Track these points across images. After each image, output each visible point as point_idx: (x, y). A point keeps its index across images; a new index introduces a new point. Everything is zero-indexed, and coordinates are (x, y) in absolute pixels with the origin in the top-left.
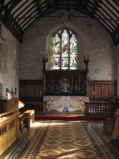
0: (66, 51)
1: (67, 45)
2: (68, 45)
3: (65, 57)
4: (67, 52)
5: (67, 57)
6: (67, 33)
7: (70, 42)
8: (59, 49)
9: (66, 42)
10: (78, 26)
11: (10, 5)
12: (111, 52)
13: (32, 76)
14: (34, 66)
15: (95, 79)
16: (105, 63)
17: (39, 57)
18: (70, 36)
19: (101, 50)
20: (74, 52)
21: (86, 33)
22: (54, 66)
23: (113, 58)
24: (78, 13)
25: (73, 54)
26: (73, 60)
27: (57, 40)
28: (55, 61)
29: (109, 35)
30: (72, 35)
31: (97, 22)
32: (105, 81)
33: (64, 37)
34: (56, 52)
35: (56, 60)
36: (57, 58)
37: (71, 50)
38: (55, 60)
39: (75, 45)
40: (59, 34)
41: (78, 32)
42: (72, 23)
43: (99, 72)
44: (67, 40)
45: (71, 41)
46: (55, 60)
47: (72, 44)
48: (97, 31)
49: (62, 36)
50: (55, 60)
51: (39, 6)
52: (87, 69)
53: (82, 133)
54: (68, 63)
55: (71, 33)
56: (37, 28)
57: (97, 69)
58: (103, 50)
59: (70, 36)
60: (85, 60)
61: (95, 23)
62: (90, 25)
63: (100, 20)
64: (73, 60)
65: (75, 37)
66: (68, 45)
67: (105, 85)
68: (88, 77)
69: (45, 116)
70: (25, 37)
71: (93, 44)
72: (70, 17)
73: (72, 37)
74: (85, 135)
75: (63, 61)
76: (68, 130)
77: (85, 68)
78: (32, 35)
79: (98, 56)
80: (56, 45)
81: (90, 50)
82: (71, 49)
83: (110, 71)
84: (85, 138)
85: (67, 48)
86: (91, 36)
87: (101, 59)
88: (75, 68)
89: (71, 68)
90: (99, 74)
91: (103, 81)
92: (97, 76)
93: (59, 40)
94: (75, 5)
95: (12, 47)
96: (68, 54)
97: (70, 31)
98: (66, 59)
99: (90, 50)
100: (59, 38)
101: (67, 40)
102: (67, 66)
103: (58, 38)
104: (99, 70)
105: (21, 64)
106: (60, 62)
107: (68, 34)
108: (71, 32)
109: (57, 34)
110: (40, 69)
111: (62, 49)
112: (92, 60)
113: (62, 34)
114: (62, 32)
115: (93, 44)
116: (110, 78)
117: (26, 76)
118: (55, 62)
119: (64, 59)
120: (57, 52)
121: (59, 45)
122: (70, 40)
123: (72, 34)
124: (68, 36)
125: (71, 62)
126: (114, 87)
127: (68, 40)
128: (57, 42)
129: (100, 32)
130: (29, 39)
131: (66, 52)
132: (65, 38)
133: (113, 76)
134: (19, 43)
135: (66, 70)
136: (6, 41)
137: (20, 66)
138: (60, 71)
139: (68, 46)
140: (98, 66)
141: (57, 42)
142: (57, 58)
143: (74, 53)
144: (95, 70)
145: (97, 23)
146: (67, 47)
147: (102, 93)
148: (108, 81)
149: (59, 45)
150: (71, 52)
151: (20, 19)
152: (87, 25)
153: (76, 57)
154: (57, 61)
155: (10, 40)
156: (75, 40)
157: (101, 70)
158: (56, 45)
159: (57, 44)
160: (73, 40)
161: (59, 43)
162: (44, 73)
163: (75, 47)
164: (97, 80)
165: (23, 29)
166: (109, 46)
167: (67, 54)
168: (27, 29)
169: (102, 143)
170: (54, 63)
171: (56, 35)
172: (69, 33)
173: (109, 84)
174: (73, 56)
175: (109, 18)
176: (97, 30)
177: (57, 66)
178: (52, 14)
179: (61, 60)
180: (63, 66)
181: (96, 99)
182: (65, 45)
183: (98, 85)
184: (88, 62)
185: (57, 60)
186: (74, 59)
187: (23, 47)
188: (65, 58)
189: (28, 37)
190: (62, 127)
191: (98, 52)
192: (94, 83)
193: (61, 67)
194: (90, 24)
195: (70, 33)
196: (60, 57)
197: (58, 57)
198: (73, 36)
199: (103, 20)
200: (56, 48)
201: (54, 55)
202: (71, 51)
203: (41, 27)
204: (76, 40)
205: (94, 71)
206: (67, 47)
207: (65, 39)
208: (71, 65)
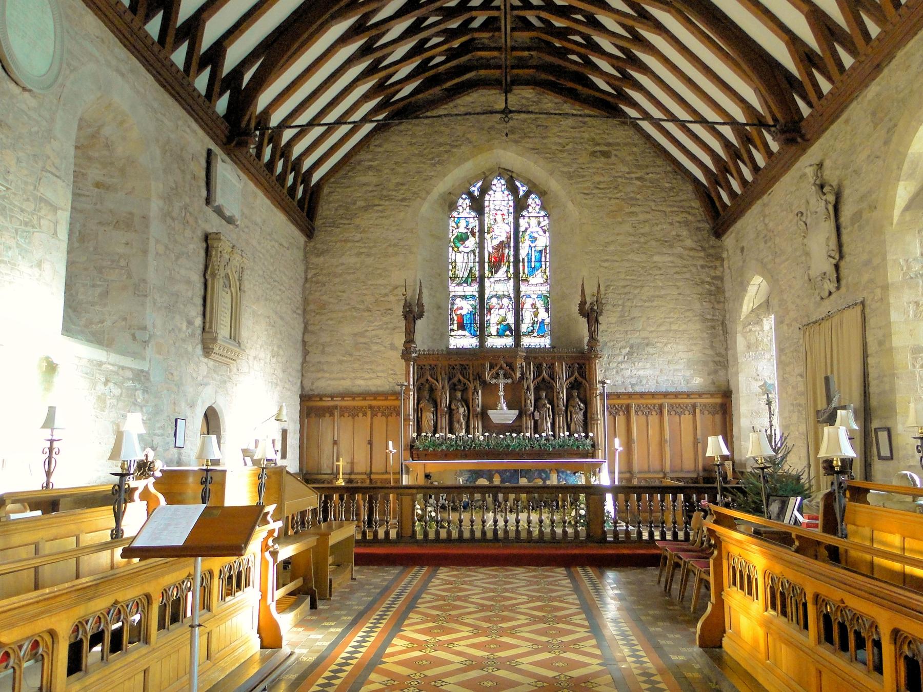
0: (504, 269)
1: (509, 243)
2: (512, 245)
3: (502, 293)
4: (507, 271)
5: (508, 296)
7: (522, 229)
9: (501, 231)
10: (553, 162)
11: (249, 69)
12: (703, 267)
13: (356, 378)
14: (368, 334)
16: (676, 316)
17: (386, 295)
18: (520, 206)
19: (656, 258)
21: (589, 188)
22: (453, 333)
23: (710, 293)
24: (550, 102)
25: (532, 280)
26: (534, 306)
27: (463, 224)
28: (459, 312)
29: (687, 193)
30: (530, 201)
31: (636, 138)
32: (676, 395)
33: (492, 207)
34: (462, 273)
35: (462, 308)
36: (465, 297)
37: (526, 264)
39: (543, 241)
40: (470, 195)
41: (554, 185)
42: (527, 145)
43: (649, 354)
44: (506, 221)
45: (523, 223)
46: (455, 307)
47: (527, 237)
48: (637, 179)
49: (486, 203)
50: (455, 307)
51: (382, 74)
52: (593, 339)
53: (566, 619)
54: (511, 319)
55: (522, 190)
57: (639, 341)
58: (667, 259)
59: (520, 206)
60: (585, 303)
61: (626, 144)
62: (606, 154)
63: (646, 125)
64: (534, 306)
65: (543, 208)
66: (512, 245)
67: (679, 410)
68: (599, 378)
70: (326, 210)
72: (510, 116)
73: (530, 209)
74: (578, 629)
75: (490, 310)
76: (506, 608)
77: (586, 339)
78: (355, 204)
79: (642, 287)
80: (458, 245)
81: (607, 260)
82: (526, 260)
84: (575, 642)
85: (509, 256)
86: (610, 199)
87: (658, 296)
88: (542, 339)
89: (526, 341)
90: (648, 365)
91: (666, 395)
92: (641, 372)
93: (474, 223)
95: (267, 251)
97: (520, 182)
98: (505, 301)
99: (607, 260)
100: (473, 214)
101: (506, 221)
102: (508, 333)
104: (647, 345)
105: (309, 328)
106: (477, 318)
107: (511, 197)
108: (524, 188)
109: (464, 196)
111: (486, 260)
113: (487, 197)
114: (484, 190)
116: (697, 382)
117: (330, 379)
119: (494, 301)
120: (466, 275)
121: (471, 243)
122: (521, 221)
123: (527, 195)
124: (511, 203)
125: (527, 316)
126: (718, 418)
127: (511, 219)
128: (465, 231)
129: (651, 182)
130: (341, 218)
131: (501, 274)
132: (499, 212)
133: (716, 372)
134: (301, 239)
135: (504, 350)
136: (237, 226)
137: (304, 334)
138: (481, 353)
139: (509, 247)
140: (644, 329)
141: (462, 230)
142: (465, 297)
143: (538, 278)
144: (631, 347)
145: (635, 145)
147: (667, 447)
148: (688, 395)
149: (471, 243)
151: (304, 130)
152: (593, 154)
153: (545, 293)
154: (464, 312)
155: (259, 220)
156: (541, 219)
157: (658, 345)
158: (458, 245)
159: (462, 239)
160: (534, 222)
161: (473, 234)
162: (408, 366)
163: (541, 252)
164: (638, 389)
165: (316, 177)
166: (689, 243)
168: (332, 176)
169: (650, 665)
170: (452, 319)
171: (461, 201)
172: (513, 190)
173: (694, 406)
174: (533, 288)
175: (682, 115)
176: (637, 175)
177: (466, 333)
178: (441, 111)
179: (482, 307)
180: (490, 335)
181: (640, 472)
182: (496, 242)
183: (645, 411)
184: (599, 313)
185: (465, 307)
186: (540, 304)
187: (318, 256)
188: (499, 297)
189: (336, 210)
190: (479, 596)
191: (643, 267)
193: (482, 340)
194: (606, 149)
195: (521, 193)
196: (476, 294)
197: (467, 293)
198: (534, 205)
199: (656, 123)
200: (459, 258)
201: (454, 289)
202: (524, 269)
204: (547, 222)
205: (628, 349)
207: (499, 218)
208: (524, 328)
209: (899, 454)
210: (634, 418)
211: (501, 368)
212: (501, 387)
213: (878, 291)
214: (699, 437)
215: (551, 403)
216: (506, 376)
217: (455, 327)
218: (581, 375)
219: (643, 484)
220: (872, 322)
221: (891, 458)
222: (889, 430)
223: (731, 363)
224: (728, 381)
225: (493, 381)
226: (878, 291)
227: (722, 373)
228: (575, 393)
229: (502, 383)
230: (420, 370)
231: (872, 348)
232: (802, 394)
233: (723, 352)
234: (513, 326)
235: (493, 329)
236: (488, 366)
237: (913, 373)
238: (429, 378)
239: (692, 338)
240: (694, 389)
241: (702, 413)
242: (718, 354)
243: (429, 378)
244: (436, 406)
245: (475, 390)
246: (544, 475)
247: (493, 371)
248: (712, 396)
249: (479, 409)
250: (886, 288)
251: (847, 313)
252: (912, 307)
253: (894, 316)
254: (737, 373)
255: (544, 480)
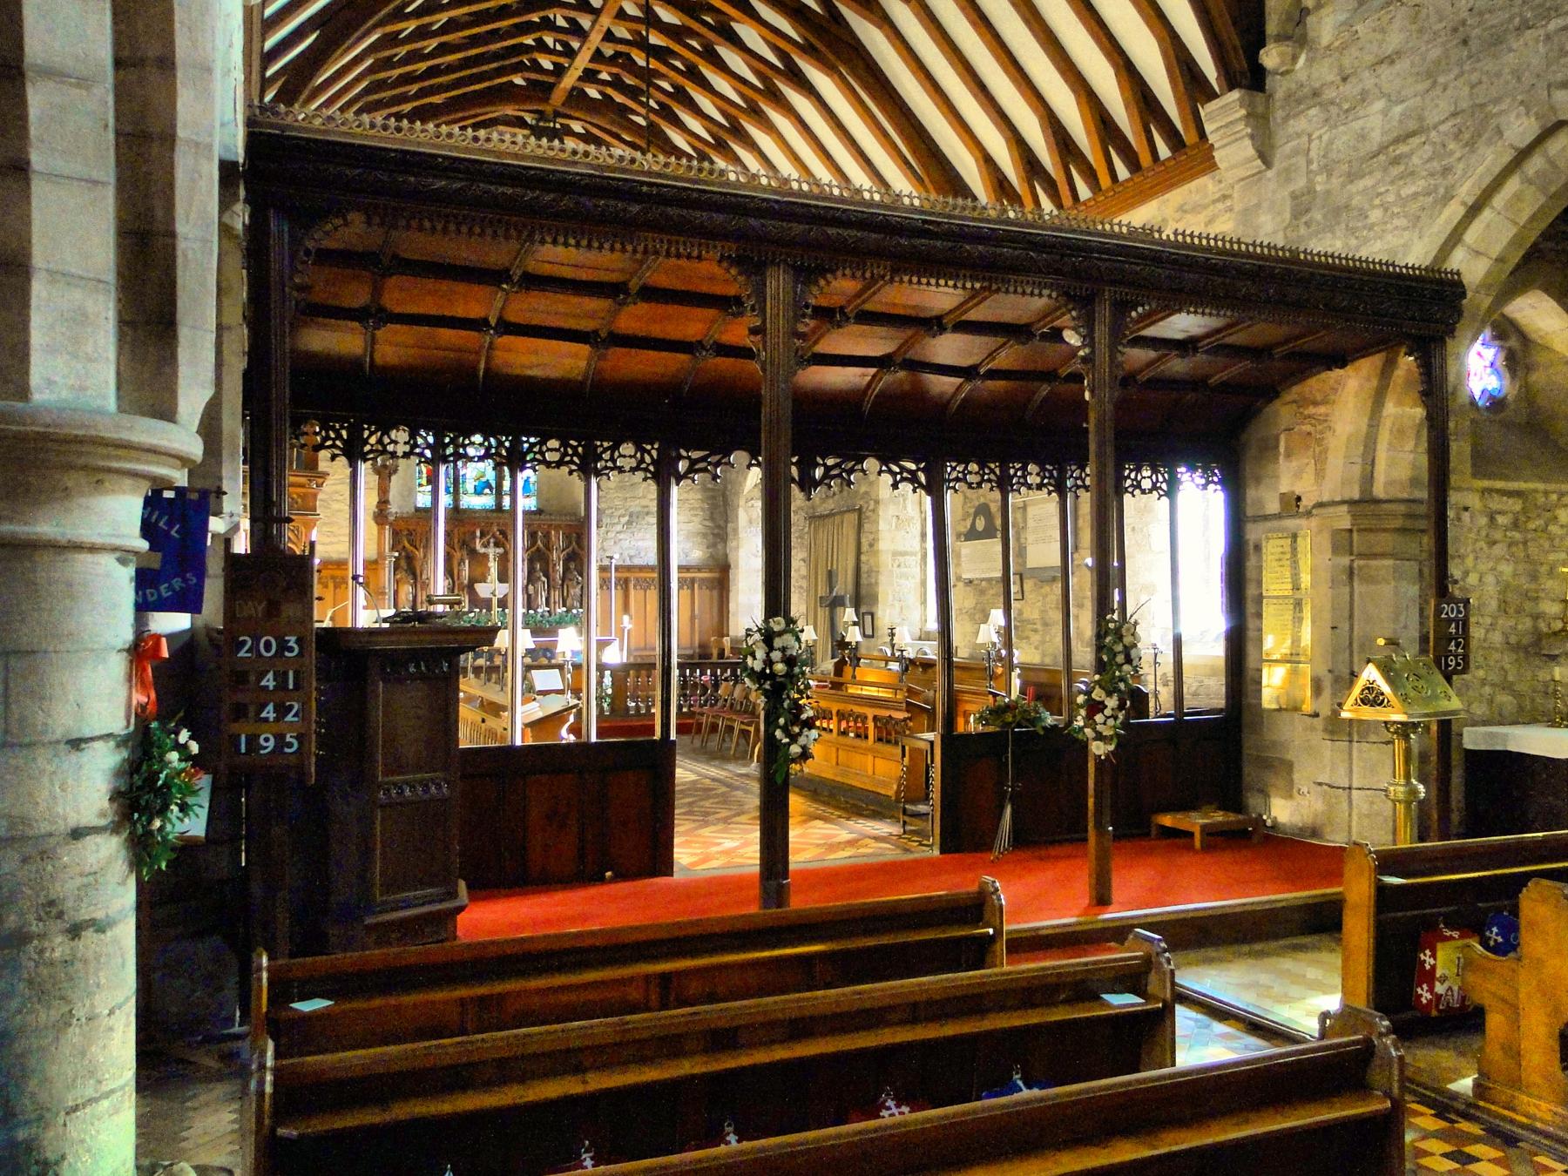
15: (631, 557)
22: (421, 489)
57: (638, 509)
69: (356, 108)
83: (697, 520)
92: (640, 543)
94: (770, 128)
102: (487, 491)
126: (715, 593)
144: (631, 516)
164: (637, 562)
173: (693, 581)
192: (627, 575)
205: (627, 518)
209: (879, 633)
210: (632, 592)
211: (494, 536)
212: (491, 557)
213: (872, 503)
214: (697, 612)
215: (546, 575)
216: (497, 545)
217: (424, 481)
218: (578, 543)
219: (639, 661)
220: (866, 526)
221: (873, 636)
222: (872, 615)
223: (730, 537)
224: (726, 555)
225: (483, 550)
226: (872, 503)
227: (720, 547)
228: (572, 566)
229: (492, 552)
230: (396, 534)
231: (865, 548)
232: (804, 577)
233: (722, 523)
234: (494, 485)
235: (470, 486)
236: (478, 534)
237: (891, 571)
238: (407, 545)
239: (693, 509)
240: (693, 563)
241: (700, 588)
242: (719, 527)
243: (407, 545)
244: (415, 578)
245: (462, 561)
246: (549, 654)
247: (485, 540)
248: (711, 571)
249: (466, 582)
250: (877, 502)
251: (846, 516)
252: (895, 519)
253: (882, 526)
254: (737, 548)
255: (550, 659)
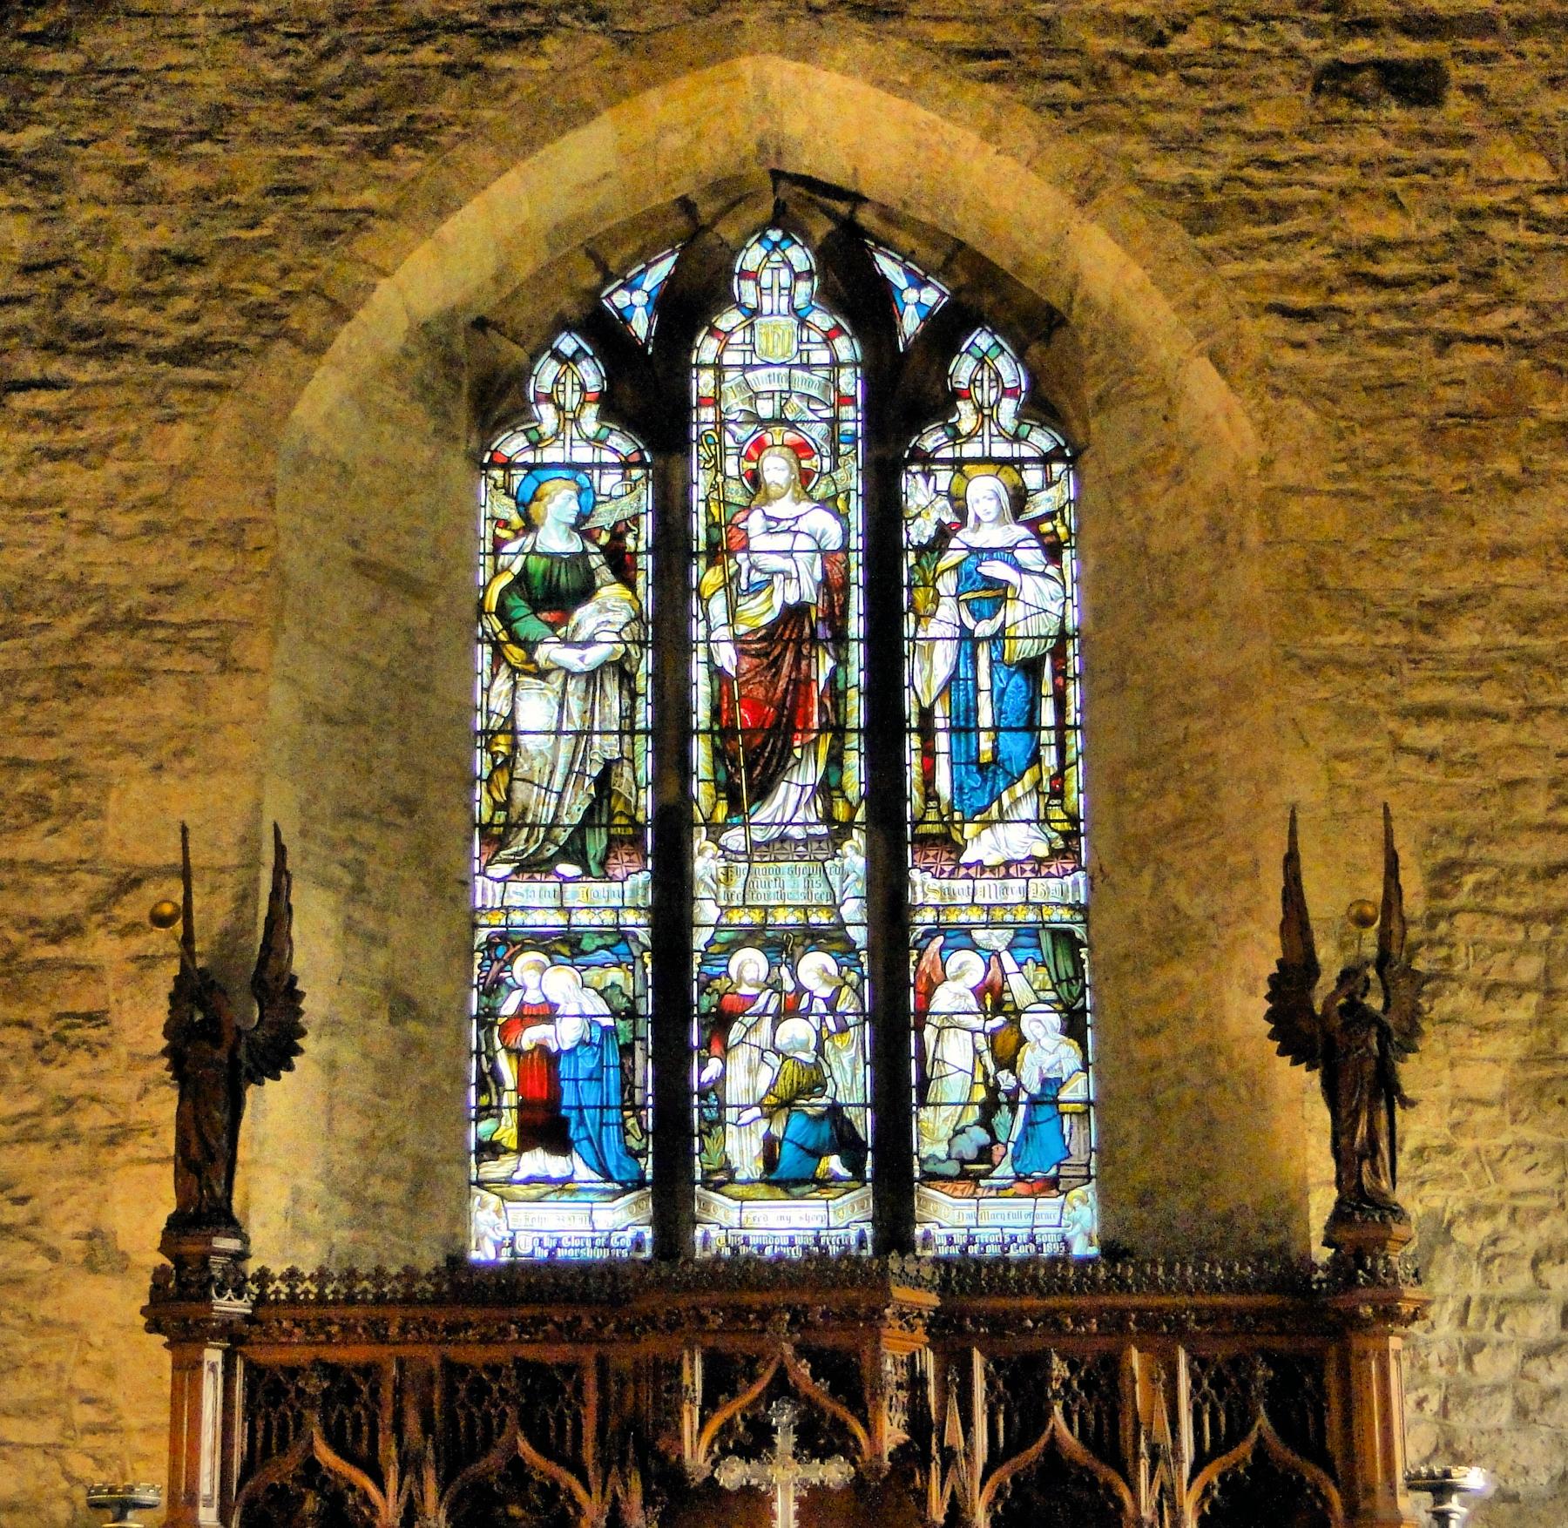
1: (836, 618)
4: (827, 789)
5: (829, 937)
6: (823, 320)
7: (919, 531)
8: (628, 731)
20: (1022, 800)
21: (1313, 280)
22: (494, 1170)
25: (983, 846)
27: (559, 504)
28: (530, 1037)
30: (963, 370)
33: (734, 403)
38: (525, 1016)
47: (947, 584)
49: (703, 383)
50: (509, 1007)
56: (45, 181)
71: (1502, 552)
73: (966, 417)
75: (721, 1021)
77: (1322, 1202)
81: (1436, 712)
85: (836, 693)
88: (1048, 1207)
96: (854, 856)
100: (622, 444)
103: (583, 454)
106: (644, 1070)
107: (846, 348)
109: (567, 344)
110: (91, 1265)
111: (702, 715)
112: (1490, 991)
113: (707, 349)
115: (1502, 552)
118: (508, 1070)
119: (750, 964)
124: (849, 382)
127: (851, 476)
132: (776, 435)
139: (840, 639)
141: (555, 538)
146: (826, 664)
150: (943, 784)
153: (1059, 916)
154: (565, 1034)
158: (530, 626)
160: (984, 491)
162: (187, 1371)
163: (1030, 667)
167: (842, 832)
170: (489, 1081)
171: (547, 371)
174: (988, 891)
177: (575, 1166)
180: (723, 1178)
182: (759, 612)
194: (1411, 50)
195: (910, 323)
203: (131, 175)
206: (826, 664)
207: (776, 469)
